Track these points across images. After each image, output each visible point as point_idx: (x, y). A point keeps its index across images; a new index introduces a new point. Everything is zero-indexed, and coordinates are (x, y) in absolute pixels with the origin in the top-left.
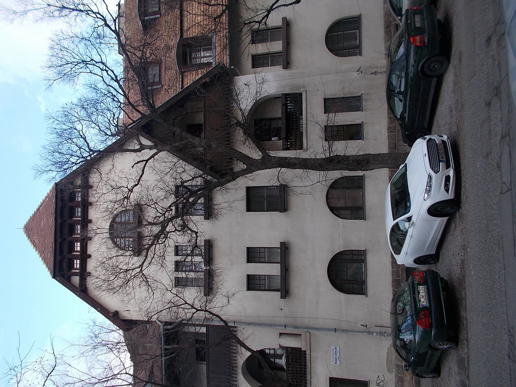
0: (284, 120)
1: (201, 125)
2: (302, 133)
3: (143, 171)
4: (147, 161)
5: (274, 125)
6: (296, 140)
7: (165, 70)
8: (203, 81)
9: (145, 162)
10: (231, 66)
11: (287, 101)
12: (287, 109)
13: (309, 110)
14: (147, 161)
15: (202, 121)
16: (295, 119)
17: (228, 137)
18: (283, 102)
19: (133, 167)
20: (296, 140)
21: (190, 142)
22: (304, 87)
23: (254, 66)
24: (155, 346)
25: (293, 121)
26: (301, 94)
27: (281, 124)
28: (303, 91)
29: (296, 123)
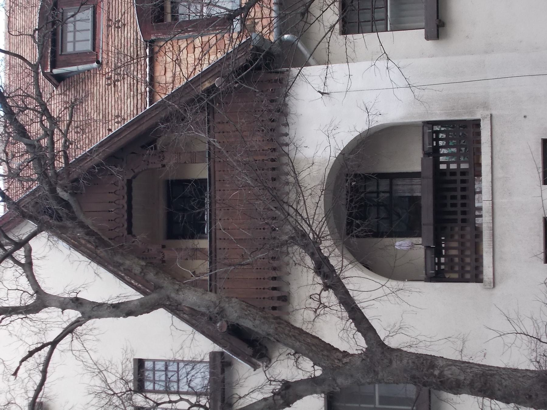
0: (429, 182)
1: (203, 181)
2: (478, 233)
3: (44, 372)
4: (54, 344)
5: (403, 189)
6: (462, 252)
7: (108, 26)
8: (207, 85)
9: (47, 349)
10: (281, 33)
11: (438, 139)
12: (437, 163)
13: (499, 173)
14: (54, 344)
15: (205, 175)
16: (459, 194)
17: (274, 278)
18: (428, 146)
19: (15, 374)
20: (462, 252)
21: (169, 298)
22: (485, 106)
23: (348, 26)
24: (137, 361)
25: (454, 197)
26: (476, 124)
27: (423, 191)
28: (485, 118)
29: (464, 205)
